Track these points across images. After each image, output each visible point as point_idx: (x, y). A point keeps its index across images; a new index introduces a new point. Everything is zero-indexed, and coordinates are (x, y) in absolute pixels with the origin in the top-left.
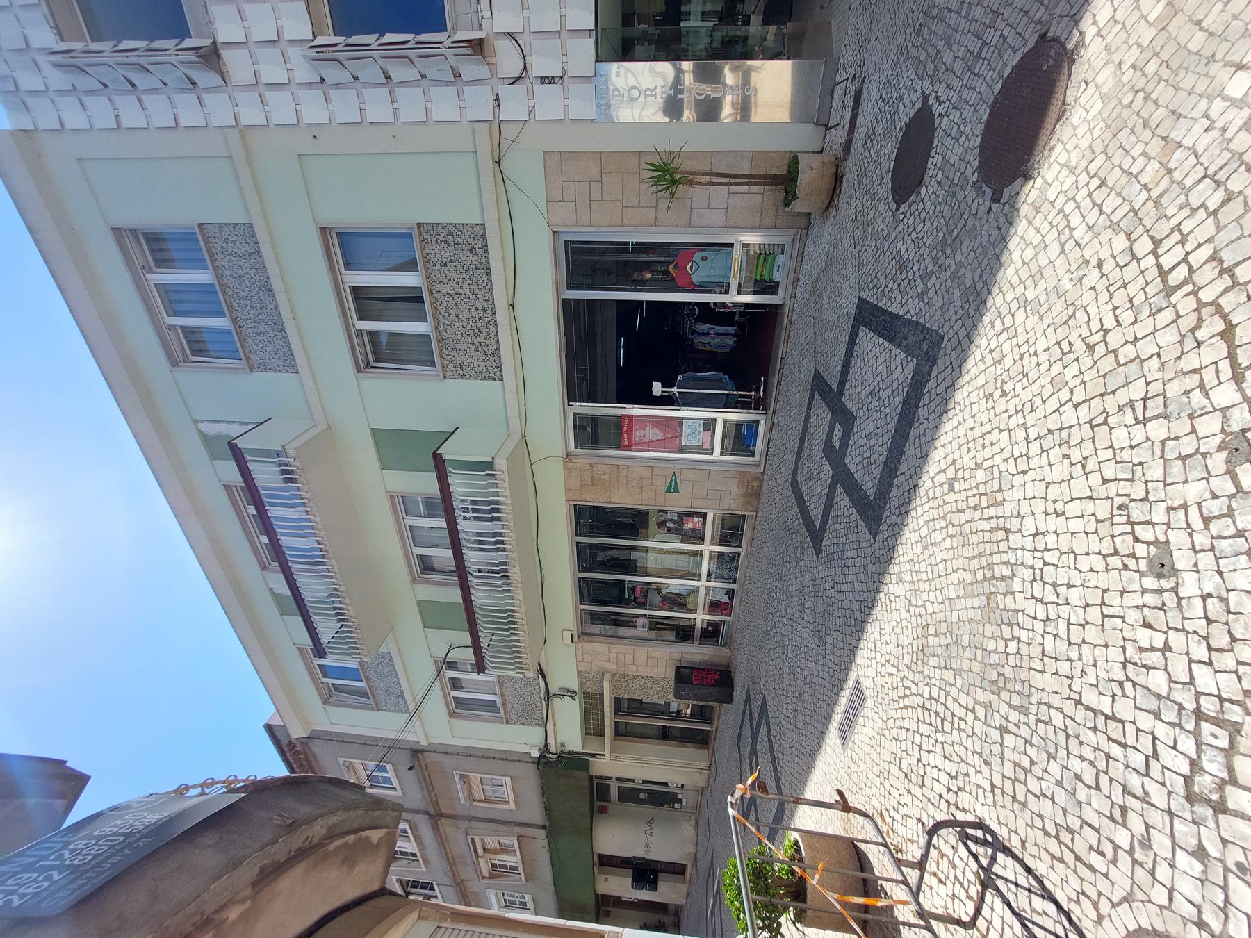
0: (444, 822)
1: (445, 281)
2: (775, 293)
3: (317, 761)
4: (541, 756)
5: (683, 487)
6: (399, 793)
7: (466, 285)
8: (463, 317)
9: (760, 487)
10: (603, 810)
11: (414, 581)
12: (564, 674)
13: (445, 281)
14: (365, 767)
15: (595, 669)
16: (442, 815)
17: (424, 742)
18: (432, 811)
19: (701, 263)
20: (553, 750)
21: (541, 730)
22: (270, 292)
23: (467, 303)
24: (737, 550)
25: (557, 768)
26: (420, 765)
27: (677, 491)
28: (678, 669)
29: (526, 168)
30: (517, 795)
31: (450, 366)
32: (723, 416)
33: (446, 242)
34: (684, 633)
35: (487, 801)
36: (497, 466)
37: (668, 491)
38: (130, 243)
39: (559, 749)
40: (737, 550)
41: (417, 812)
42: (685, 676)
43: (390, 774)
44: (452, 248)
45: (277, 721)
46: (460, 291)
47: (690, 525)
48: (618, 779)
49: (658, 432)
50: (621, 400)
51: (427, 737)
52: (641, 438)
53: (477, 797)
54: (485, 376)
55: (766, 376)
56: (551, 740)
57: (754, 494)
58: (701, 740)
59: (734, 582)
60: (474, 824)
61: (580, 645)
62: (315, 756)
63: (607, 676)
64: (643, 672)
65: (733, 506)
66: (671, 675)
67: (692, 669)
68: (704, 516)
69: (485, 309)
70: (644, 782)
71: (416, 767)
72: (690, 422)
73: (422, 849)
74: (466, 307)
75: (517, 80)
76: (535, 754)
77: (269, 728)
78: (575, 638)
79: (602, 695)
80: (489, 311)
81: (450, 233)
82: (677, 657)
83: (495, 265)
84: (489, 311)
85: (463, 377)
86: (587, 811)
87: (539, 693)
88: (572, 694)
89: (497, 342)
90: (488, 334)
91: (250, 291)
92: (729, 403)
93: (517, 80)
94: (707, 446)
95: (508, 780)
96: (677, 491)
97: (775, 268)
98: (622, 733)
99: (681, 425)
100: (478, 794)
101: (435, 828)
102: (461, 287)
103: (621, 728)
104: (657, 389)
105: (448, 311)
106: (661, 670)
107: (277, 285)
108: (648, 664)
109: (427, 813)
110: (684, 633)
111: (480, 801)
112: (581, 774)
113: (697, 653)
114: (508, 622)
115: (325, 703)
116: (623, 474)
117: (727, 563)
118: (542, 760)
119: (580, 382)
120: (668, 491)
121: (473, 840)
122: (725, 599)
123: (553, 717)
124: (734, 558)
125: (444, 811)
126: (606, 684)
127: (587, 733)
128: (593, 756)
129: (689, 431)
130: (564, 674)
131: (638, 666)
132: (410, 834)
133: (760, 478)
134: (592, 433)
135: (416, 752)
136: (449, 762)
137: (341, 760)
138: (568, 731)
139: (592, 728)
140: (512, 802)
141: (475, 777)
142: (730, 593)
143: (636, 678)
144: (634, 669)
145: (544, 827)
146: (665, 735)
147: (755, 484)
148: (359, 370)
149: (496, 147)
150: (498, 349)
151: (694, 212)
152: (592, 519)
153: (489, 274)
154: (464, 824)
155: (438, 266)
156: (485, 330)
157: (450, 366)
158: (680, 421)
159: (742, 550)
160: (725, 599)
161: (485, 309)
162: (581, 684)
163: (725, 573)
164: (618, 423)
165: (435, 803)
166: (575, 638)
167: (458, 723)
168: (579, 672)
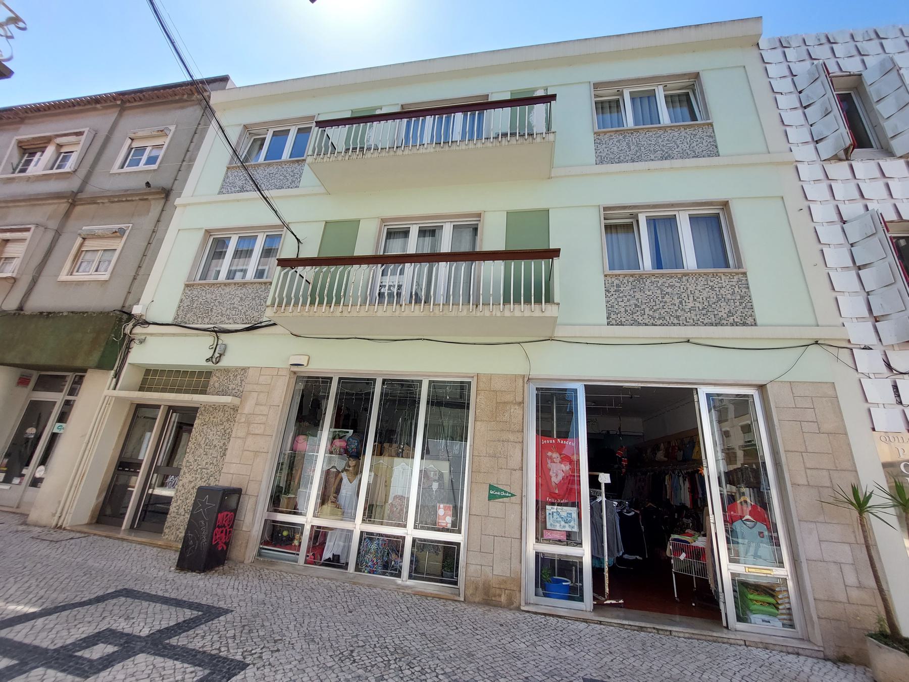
0: (64, 206)
1: (699, 288)
2: (740, 619)
3: (176, 109)
4: (130, 316)
5: (496, 505)
6: (115, 169)
7: (697, 305)
8: (667, 298)
9: (498, 605)
10: (23, 381)
11: (383, 220)
12: (241, 352)
13: (699, 288)
14: (159, 147)
15: (248, 388)
16: (73, 205)
17: (178, 201)
18: (80, 196)
19: (756, 530)
20: (138, 330)
21: (170, 321)
22: (664, 158)
23: (681, 303)
24: (405, 572)
25: (111, 333)
26: (150, 194)
27: (491, 497)
28: (238, 492)
29: (816, 366)
30: (82, 279)
31: (616, 282)
32: (585, 553)
33: (733, 293)
34: (283, 495)
35: (79, 252)
36: (549, 306)
37: (491, 487)
38: (685, 82)
39: (137, 337)
40: (405, 572)
41: (85, 182)
42: (222, 504)
43: (142, 166)
44: (729, 297)
45: (229, 85)
46: (691, 298)
47: (441, 512)
48: (68, 404)
49: (560, 478)
50: (589, 434)
51: (185, 206)
52: (551, 458)
53: (87, 243)
54: (610, 311)
55: (625, 606)
56: (152, 329)
57: (489, 597)
58: (108, 512)
59: (357, 569)
60: (50, 235)
61: (285, 373)
62: (182, 108)
63: (237, 401)
64: (234, 446)
65: (472, 568)
66: (225, 481)
67: (235, 511)
68: (455, 527)
69: (678, 317)
70: (54, 437)
71: (148, 190)
72: (575, 515)
73: (28, 179)
74: (677, 302)
75: (888, 365)
76: (136, 310)
77: (225, 79)
78: (295, 369)
79: (204, 392)
80: (676, 321)
81: (742, 297)
82: (251, 489)
83: (727, 331)
84: (676, 321)
85: (607, 291)
86: (31, 361)
87: (221, 322)
88: (215, 358)
89: (646, 325)
90: (654, 318)
91: (663, 146)
92: (596, 558)
93: (888, 365)
94: (547, 535)
95: (106, 277)
96: (491, 497)
97: (766, 618)
98: (140, 415)
99: (573, 505)
100: (90, 245)
101: (58, 196)
102: (695, 300)
103: (149, 413)
104: (605, 478)
105: (672, 286)
106: (234, 469)
107: (666, 163)
108: (241, 452)
109: (81, 190)
110: (283, 495)
111: (82, 245)
112: (96, 357)
113: (253, 518)
114: (336, 297)
115: (245, 127)
116: (511, 437)
117: (384, 555)
118: (125, 317)
119: (606, 401)
120: (491, 487)
121: (28, 230)
122: (327, 554)
123: (186, 335)
124: (390, 568)
125: (78, 209)
126: (227, 399)
127: (148, 372)
128: (117, 375)
129: (564, 514)
130: (241, 352)
131: (244, 439)
132: (54, 171)
133: (511, 605)
134: (553, 405)
135: (166, 194)
136: (147, 222)
137: (173, 128)
138: (151, 351)
139: (152, 378)
140: (70, 278)
141: (118, 244)
142: (336, 562)
143: (227, 435)
144: (241, 433)
145: (21, 308)
146: (126, 465)
147: (503, 599)
148: (605, 209)
149: (827, 342)
150: (639, 324)
151: (813, 526)
152: (453, 401)
153: (711, 324)
154: (53, 224)
155: (712, 284)
156: (657, 315)
157: (616, 282)
158: (577, 504)
159: (404, 580)
160: (327, 554)
161: (678, 317)
162: (227, 370)
163: (369, 557)
164: (567, 432)
165: (93, 201)
166: (295, 369)
167: (199, 236)
168: (245, 369)
